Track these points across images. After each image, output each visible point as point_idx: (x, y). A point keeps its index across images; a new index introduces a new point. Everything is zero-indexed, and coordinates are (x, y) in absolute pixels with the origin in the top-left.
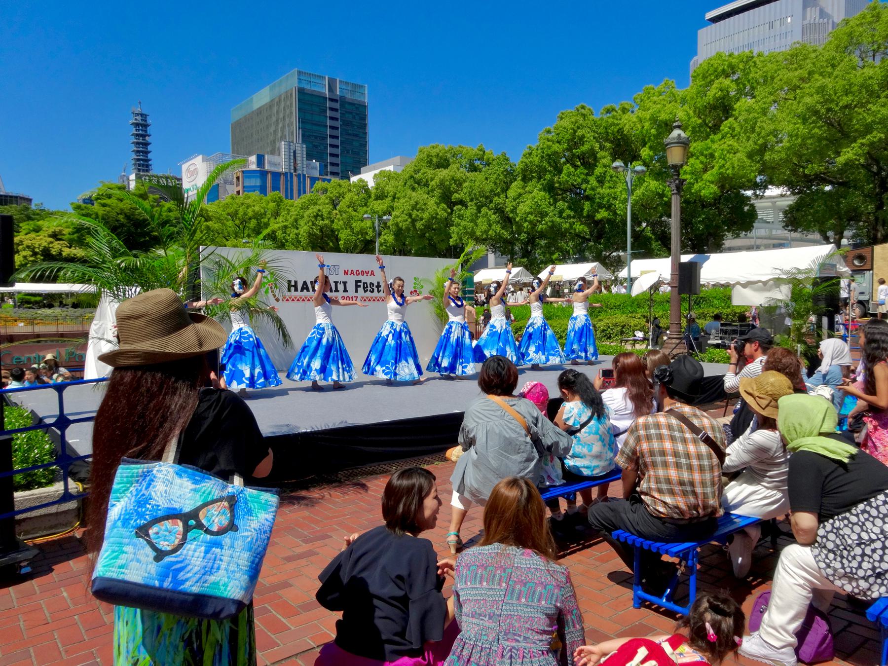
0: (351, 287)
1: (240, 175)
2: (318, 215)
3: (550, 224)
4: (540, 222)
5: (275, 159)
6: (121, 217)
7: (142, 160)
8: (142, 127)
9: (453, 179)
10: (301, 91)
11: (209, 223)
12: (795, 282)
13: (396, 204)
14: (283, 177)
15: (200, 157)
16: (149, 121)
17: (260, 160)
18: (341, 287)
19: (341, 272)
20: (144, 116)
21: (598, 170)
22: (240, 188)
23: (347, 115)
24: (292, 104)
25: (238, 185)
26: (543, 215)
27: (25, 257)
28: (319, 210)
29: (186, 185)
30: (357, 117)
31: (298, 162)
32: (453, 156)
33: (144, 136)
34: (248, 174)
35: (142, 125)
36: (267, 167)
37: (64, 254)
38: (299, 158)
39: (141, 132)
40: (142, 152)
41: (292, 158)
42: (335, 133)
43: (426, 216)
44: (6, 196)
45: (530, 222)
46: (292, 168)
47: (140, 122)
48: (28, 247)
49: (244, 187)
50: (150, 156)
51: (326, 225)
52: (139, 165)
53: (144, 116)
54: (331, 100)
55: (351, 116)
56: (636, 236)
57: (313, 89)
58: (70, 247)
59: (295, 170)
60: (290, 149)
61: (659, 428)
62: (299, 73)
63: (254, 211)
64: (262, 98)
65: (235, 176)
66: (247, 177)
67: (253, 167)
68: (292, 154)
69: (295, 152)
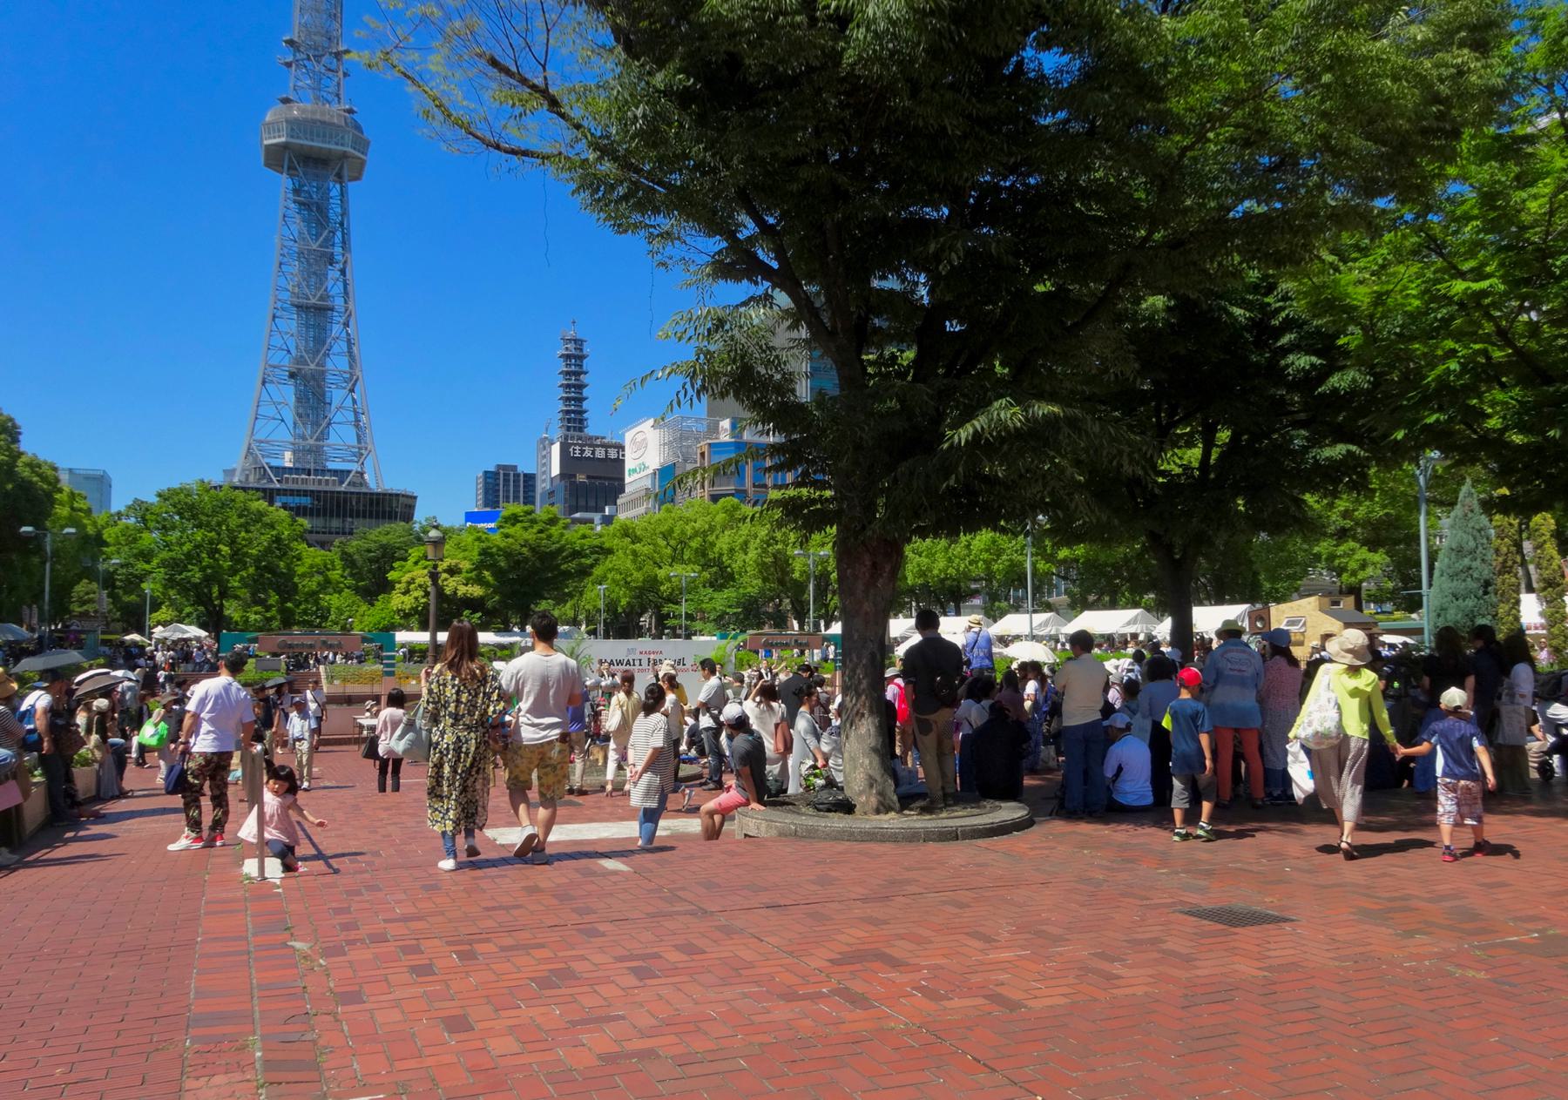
0: (645, 662)
1: (706, 449)
3: (1007, 563)
4: (996, 561)
6: (525, 550)
7: (574, 412)
8: (575, 360)
11: (637, 546)
12: (189, 698)
15: (651, 422)
16: (587, 350)
18: (637, 663)
20: (578, 342)
27: (416, 598)
29: (629, 464)
33: (577, 374)
35: (575, 357)
37: (459, 593)
39: (573, 368)
40: (574, 399)
44: (385, 495)
48: (420, 586)
50: (585, 405)
51: (779, 551)
52: (569, 420)
53: (578, 342)
58: (466, 585)
63: (693, 528)
66: (715, 453)
67: (725, 437)
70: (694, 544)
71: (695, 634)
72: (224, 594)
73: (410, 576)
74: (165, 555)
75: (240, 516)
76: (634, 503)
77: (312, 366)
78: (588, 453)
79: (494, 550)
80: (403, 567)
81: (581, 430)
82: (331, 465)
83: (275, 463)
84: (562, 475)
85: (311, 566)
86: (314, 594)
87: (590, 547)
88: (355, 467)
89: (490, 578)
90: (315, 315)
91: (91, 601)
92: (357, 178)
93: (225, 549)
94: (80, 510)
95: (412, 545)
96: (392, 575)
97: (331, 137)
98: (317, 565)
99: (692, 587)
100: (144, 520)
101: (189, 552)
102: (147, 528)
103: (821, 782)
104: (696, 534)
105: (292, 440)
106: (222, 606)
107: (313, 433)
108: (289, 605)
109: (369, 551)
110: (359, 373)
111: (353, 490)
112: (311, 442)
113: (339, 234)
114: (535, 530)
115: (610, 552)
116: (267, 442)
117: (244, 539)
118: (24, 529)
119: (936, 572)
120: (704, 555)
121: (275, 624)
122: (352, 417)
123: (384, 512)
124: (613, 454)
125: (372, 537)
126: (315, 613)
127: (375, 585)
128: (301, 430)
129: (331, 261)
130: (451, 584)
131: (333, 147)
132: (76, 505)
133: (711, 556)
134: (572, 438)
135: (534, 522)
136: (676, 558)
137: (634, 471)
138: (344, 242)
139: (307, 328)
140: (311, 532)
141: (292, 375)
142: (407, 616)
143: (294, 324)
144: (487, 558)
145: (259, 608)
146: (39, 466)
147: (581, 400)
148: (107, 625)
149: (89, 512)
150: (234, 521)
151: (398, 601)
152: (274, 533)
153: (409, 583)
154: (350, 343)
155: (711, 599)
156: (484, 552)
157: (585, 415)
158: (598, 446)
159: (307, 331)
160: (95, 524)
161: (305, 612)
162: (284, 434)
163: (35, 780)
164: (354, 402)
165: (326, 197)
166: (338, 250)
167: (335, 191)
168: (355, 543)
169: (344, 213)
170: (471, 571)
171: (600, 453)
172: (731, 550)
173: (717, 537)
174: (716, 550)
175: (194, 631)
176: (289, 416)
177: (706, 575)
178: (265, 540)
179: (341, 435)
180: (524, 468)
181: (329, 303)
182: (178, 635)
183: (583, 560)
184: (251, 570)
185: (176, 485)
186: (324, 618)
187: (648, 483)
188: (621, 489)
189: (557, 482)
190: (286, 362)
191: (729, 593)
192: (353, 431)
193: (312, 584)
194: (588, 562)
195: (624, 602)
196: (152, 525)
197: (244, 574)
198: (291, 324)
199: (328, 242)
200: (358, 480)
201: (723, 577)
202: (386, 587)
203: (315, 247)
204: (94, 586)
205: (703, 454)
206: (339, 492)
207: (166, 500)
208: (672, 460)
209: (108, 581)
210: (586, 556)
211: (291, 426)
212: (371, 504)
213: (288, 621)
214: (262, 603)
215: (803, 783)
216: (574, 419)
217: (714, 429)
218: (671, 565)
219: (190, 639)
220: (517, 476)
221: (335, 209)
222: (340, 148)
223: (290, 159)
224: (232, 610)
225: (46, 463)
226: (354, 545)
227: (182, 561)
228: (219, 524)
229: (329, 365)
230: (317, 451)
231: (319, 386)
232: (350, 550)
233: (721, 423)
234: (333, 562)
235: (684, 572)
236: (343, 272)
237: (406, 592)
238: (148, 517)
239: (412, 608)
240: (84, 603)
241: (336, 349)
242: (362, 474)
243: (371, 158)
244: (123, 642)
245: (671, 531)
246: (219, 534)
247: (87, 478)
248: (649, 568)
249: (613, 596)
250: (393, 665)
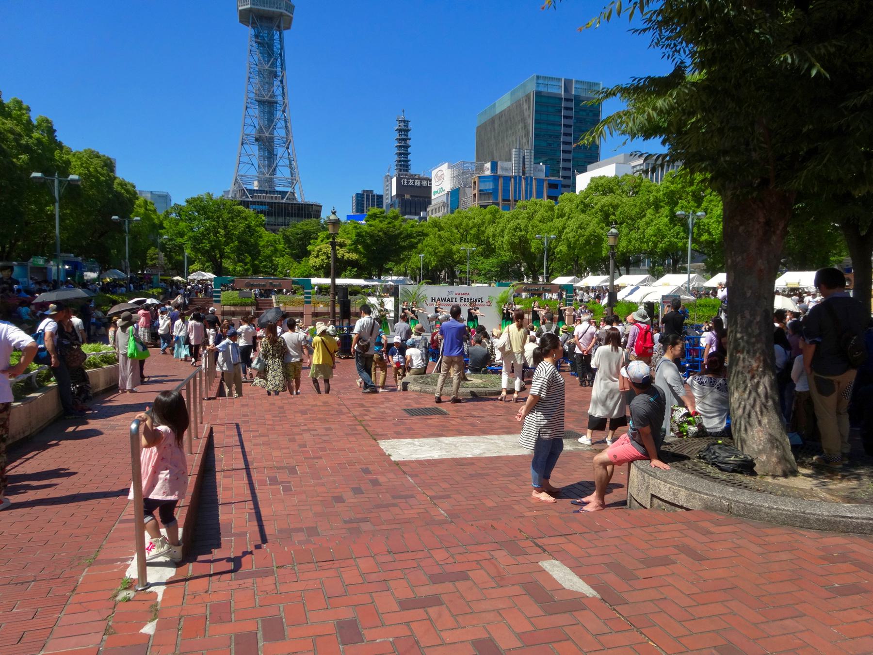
1: (477, 180)
2: (517, 228)
4: (661, 242)
5: (507, 164)
7: (403, 161)
8: (404, 131)
9: (611, 204)
10: (538, 94)
11: (442, 233)
13: (569, 222)
14: (512, 180)
15: (446, 164)
16: (410, 126)
17: (494, 168)
18: (454, 300)
19: (454, 294)
20: (406, 122)
21: (704, 204)
22: (476, 192)
23: (581, 113)
24: (529, 107)
25: (474, 189)
26: (663, 237)
27: (322, 260)
28: (518, 224)
29: (434, 188)
30: (591, 114)
31: (527, 166)
32: (617, 184)
33: (405, 140)
34: (482, 179)
35: (404, 130)
36: (499, 172)
37: (345, 257)
38: (527, 163)
40: (403, 154)
41: (521, 162)
42: (568, 130)
43: (587, 233)
45: (653, 242)
46: (521, 171)
48: (325, 253)
49: (480, 191)
50: (409, 157)
51: (523, 236)
52: (401, 166)
53: (406, 122)
54: (566, 100)
55: (584, 113)
57: (549, 91)
58: (349, 253)
59: (524, 174)
60: (520, 155)
62: (538, 77)
63: (473, 223)
64: (504, 102)
65: (473, 181)
67: (488, 173)
68: (521, 160)
69: (524, 158)
70: (473, 232)
71: (473, 282)
72: (222, 256)
73: (320, 247)
74: (191, 234)
75: (229, 213)
76: (437, 210)
77: (267, 135)
78: (411, 183)
79: (364, 233)
80: (315, 242)
81: (407, 171)
82: (277, 189)
83: (249, 187)
84: (398, 195)
85: (267, 242)
86: (269, 257)
87: (416, 232)
88: (290, 190)
89: (361, 250)
90: (268, 106)
91: (157, 258)
92: (288, 28)
93: (222, 232)
94: (150, 210)
95: (319, 231)
96: (309, 248)
97: (274, 3)
98: (271, 241)
99: (472, 255)
100: (180, 215)
101: (203, 232)
102: (182, 219)
103: (693, 429)
104: (474, 226)
105: (257, 175)
106: (221, 262)
107: (268, 171)
108: (256, 262)
109: (298, 234)
110: (291, 138)
111: (289, 202)
112: (267, 176)
113: (279, 60)
114: (386, 223)
115: (427, 235)
116: (245, 176)
117: (231, 226)
118: (114, 217)
119: (621, 249)
120: (478, 238)
121: (250, 273)
122: (287, 162)
123: (305, 214)
124: (424, 184)
125: (299, 226)
126: (271, 267)
127: (301, 253)
128: (262, 170)
129: (276, 76)
130: (341, 252)
132: (148, 208)
133: (482, 238)
134: (402, 175)
135: (385, 218)
136: (463, 239)
137: (437, 192)
138: (282, 65)
139: (264, 113)
140: (268, 224)
142: (317, 269)
143: (257, 111)
144: (360, 237)
145: (241, 264)
146: (126, 185)
147: (407, 154)
148: (165, 271)
149: (155, 211)
150: (226, 216)
151: (313, 261)
152: (247, 223)
153: (318, 251)
154: (286, 122)
155: (482, 263)
156: (359, 235)
158: (417, 179)
159: (264, 116)
160: (158, 218)
161: (265, 266)
162: (253, 172)
163: (50, 385)
164: (289, 154)
165: (272, 39)
166: (279, 69)
167: (277, 37)
168: (290, 230)
169: (282, 48)
170: (351, 245)
171: (418, 183)
172: (494, 236)
173: (486, 228)
174: (486, 235)
175: (209, 275)
176: (256, 162)
177: (480, 249)
178: (242, 226)
179: (282, 173)
180: (377, 191)
181: (275, 99)
182: (200, 278)
183: (412, 240)
184: (236, 243)
185: (196, 196)
186: (275, 270)
187: (444, 199)
188: (429, 202)
189: (394, 199)
190: (253, 132)
191: (493, 260)
192: (288, 170)
193: (268, 251)
194: (415, 241)
195: (433, 264)
196: (184, 217)
197: (232, 245)
198: (255, 111)
199: (274, 65)
200: (292, 197)
201: (489, 251)
202: (307, 254)
203: (267, 68)
204: (157, 250)
205: (475, 183)
206: (282, 203)
207: (190, 204)
208: (458, 186)
209: (163, 248)
210: (414, 237)
211: (257, 168)
212: (299, 210)
213: (256, 271)
214: (242, 261)
215: (676, 429)
216: (403, 165)
217: (481, 168)
218: (460, 244)
219: (206, 280)
221: (277, 46)
222: (278, 10)
223: (252, 17)
224: (227, 264)
225: (129, 183)
226: (290, 231)
227: (199, 237)
228: (218, 218)
229: (276, 134)
230: (270, 181)
231: (271, 145)
232: (288, 234)
233: (485, 165)
234: (279, 240)
235: (469, 248)
236: (282, 82)
237: (317, 256)
238: (182, 213)
239: (320, 265)
240: (152, 259)
241: (279, 125)
242: (293, 193)
243: (296, 17)
244: (173, 281)
245: (461, 224)
246: (218, 223)
247: (159, 196)
249: (427, 260)
250: (310, 298)
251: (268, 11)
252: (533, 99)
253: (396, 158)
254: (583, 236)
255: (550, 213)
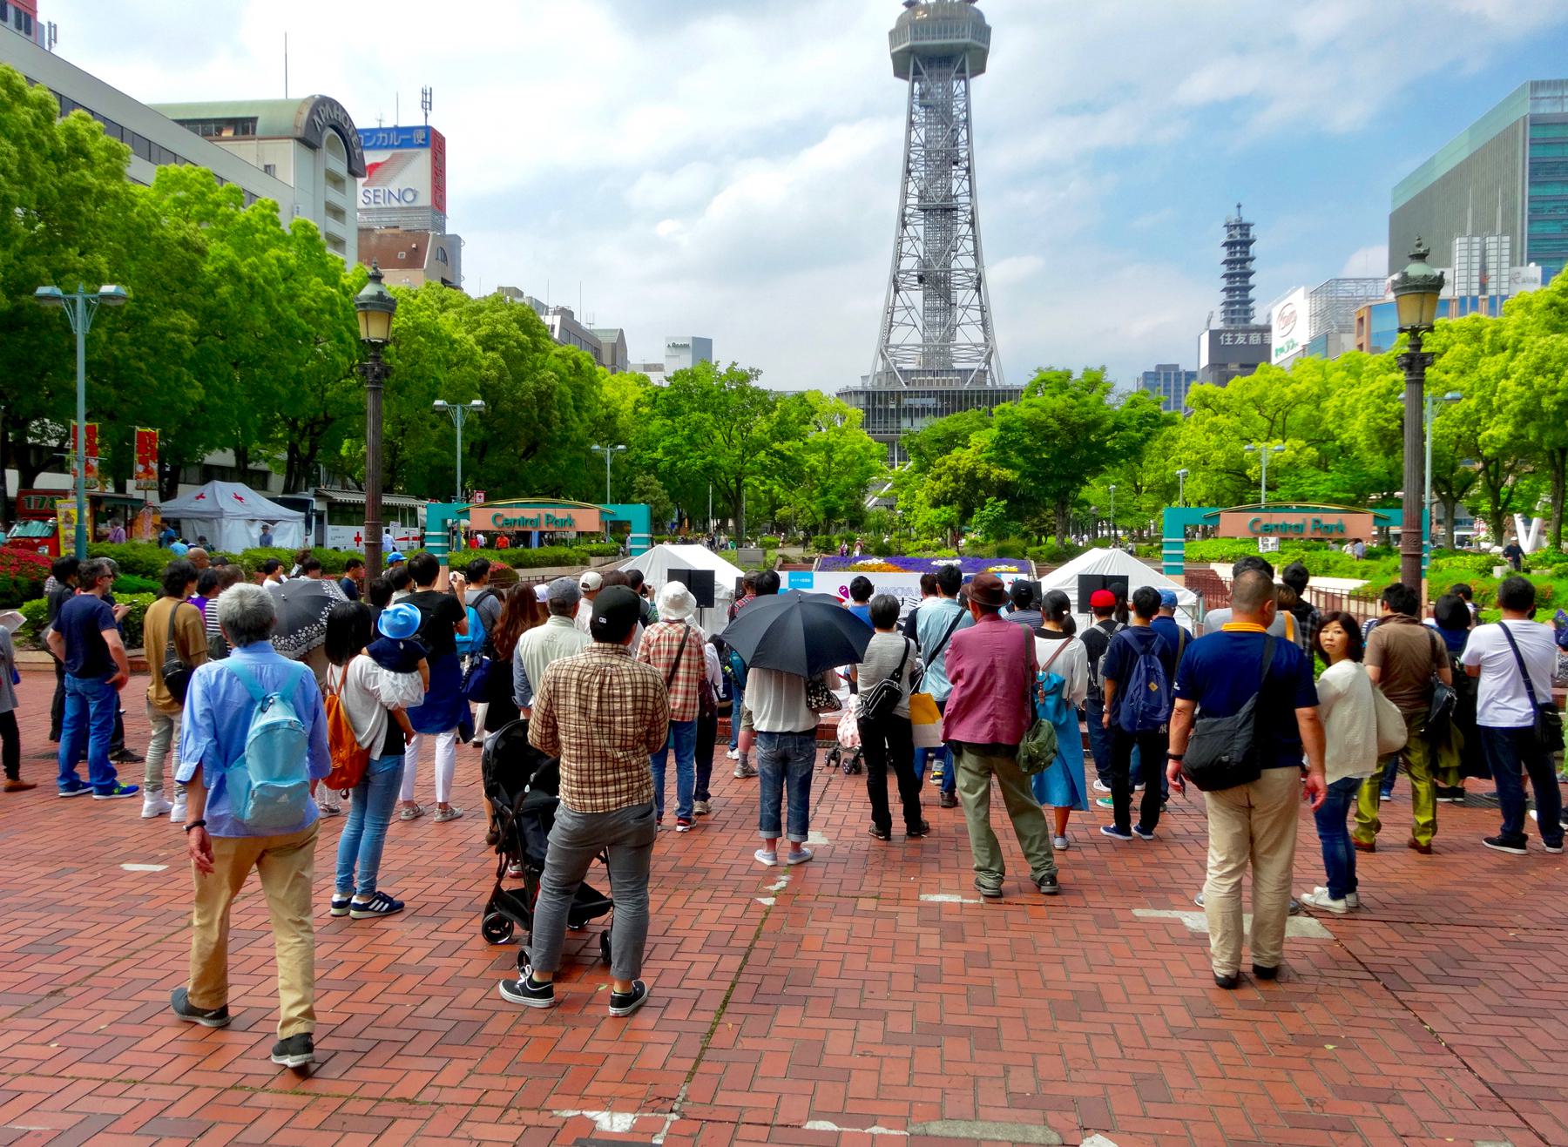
1: (1365, 314)
8: (1240, 244)
16: (1253, 232)
33: (1243, 261)
35: (1242, 243)
47: (1239, 237)
48: (950, 468)
50: (1252, 294)
53: (1244, 227)
56: (132, 441)
61: (285, 280)
78: (1241, 339)
81: (1247, 320)
82: (957, 366)
97: (952, 31)
122: (977, 316)
124: (1255, 339)
131: (954, 41)
137: (1282, 350)
141: (921, 279)
157: (1251, 305)
158: (1253, 331)
179: (968, 334)
205: (1361, 320)
220: (1178, 374)
221: (958, 107)
223: (915, 64)
241: (961, 250)
248: (1234, 445)
251: (943, 45)
252: (1524, 135)
253: (1224, 296)
254: (1554, 392)
255: (1475, 345)
